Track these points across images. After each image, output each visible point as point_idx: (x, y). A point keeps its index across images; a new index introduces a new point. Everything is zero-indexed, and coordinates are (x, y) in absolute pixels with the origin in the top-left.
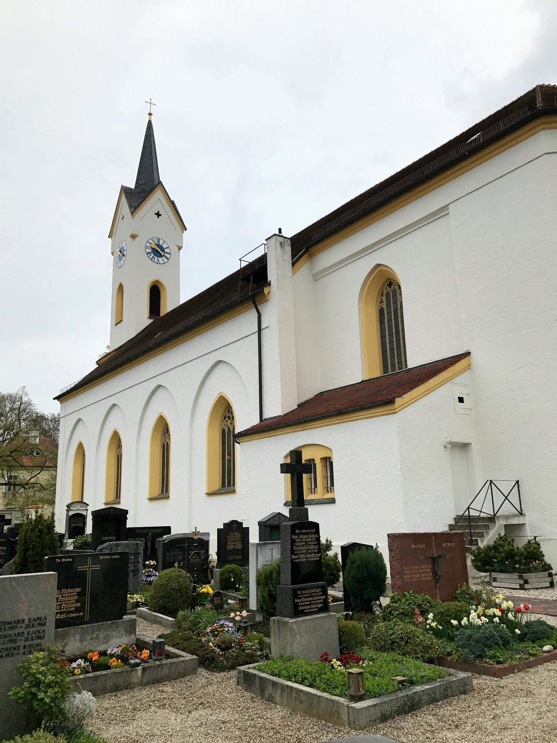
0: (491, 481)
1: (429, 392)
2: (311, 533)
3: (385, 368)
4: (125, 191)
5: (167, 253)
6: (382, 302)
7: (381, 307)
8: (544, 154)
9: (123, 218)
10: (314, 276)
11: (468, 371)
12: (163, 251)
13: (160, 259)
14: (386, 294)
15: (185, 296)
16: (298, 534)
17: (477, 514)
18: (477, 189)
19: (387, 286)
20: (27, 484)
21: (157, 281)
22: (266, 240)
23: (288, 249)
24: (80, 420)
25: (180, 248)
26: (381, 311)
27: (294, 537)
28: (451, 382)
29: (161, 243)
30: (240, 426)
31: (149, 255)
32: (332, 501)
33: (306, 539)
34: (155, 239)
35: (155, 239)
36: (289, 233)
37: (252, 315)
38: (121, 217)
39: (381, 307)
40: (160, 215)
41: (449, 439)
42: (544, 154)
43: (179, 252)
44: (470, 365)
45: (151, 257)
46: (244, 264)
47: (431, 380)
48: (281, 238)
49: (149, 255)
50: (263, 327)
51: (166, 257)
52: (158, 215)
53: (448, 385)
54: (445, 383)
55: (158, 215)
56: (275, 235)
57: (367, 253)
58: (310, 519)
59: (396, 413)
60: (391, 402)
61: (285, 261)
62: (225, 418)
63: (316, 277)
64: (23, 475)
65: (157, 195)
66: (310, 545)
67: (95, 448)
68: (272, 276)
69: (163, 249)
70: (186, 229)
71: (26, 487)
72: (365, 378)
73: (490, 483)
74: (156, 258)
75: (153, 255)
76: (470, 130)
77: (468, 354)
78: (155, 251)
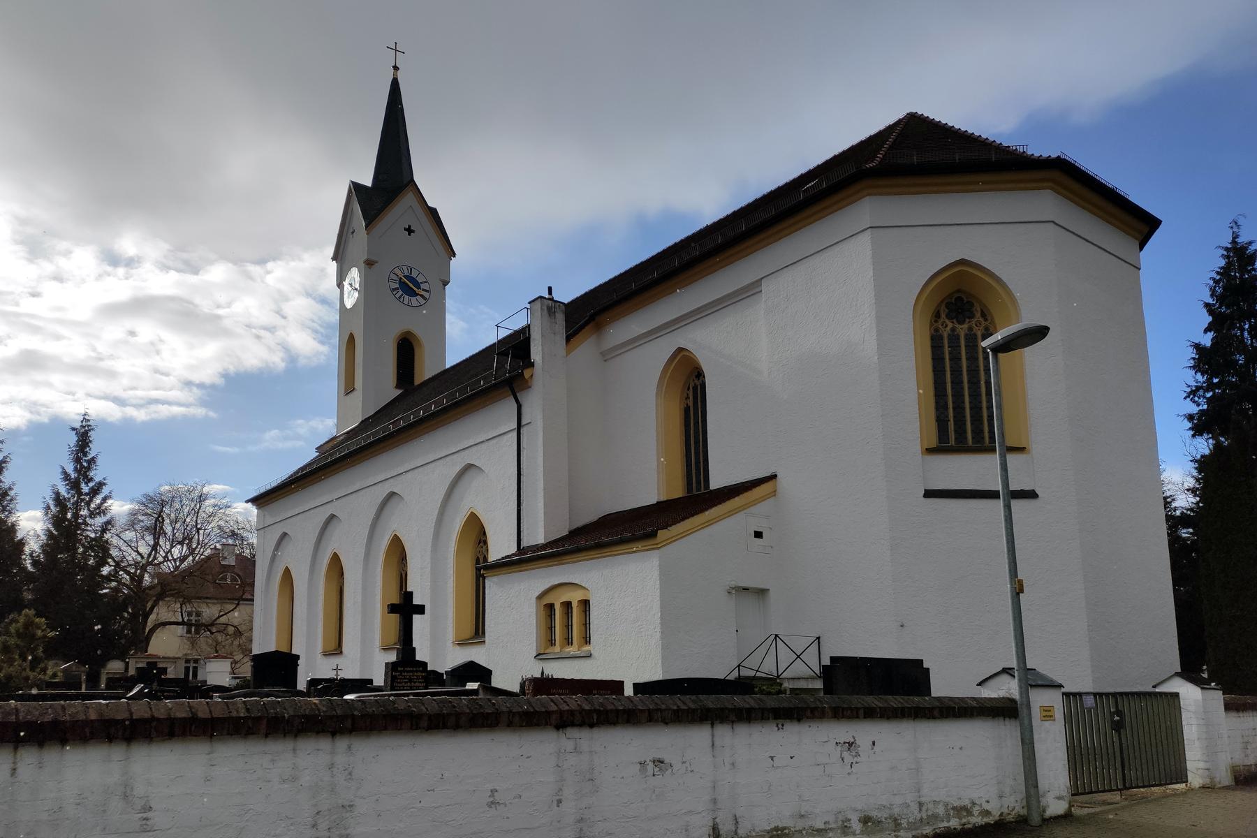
0: (776, 636)
1: (710, 523)
2: (417, 671)
3: (689, 488)
4: (356, 188)
5: (423, 290)
6: (687, 398)
7: (687, 405)
8: (868, 228)
9: (353, 233)
10: (603, 354)
11: (772, 500)
12: (419, 287)
13: (413, 299)
14: (693, 388)
15: (453, 358)
16: (401, 672)
17: (752, 673)
18: (795, 263)
19: (694, 377)
20: (213, 624)
21: (409, 333)
22: (530, 303)
23: (560, 317)
24: (285, 535)
25: (445, 283)
26: (687, 410)
27: (394, 674)
28: (745, 511)
29: (414, 275)
30: (494, 555)
31: (394, 293)
32: (589, 656)
33: (410, 676)
34: (405, 268)
35: (405, 268)
36: (567, 294)
37: (509, 406)
38: (352, 230)
39: (687, 405)
40: (413, 232)
41: (733, 583)
42: (868, 228)
43: (445, 289)
44: (775, 491)
45: (398, 296)
46: (503, 334)
47: (714, 509)
48: (550, 302)
49: (394, 293)
50: (523, 422)
51: (422, 296)
52: (410, 231)
53: (741, 516)
54: (737, 513)
55: (410, 231)
56: (541, 297)
57: (655, 337)
58: (417, 658)
59: (658, 548)
60: (653, 535)
61: (555, 334)
62: (480, 543)
63: (607, 356)
64: (209, 611)
65: (408, 199)
66: (415, 682)
67: (307, 574)
68: (536, 354)
69: (418, 285)
70: (454, 255)
71: (214, 630)
72: (663, 498)
73: (775, 638)
74: (406, 297)
75: (401, 293)
76: (802, 176)
77: (773, 477)
78: (403, 286)
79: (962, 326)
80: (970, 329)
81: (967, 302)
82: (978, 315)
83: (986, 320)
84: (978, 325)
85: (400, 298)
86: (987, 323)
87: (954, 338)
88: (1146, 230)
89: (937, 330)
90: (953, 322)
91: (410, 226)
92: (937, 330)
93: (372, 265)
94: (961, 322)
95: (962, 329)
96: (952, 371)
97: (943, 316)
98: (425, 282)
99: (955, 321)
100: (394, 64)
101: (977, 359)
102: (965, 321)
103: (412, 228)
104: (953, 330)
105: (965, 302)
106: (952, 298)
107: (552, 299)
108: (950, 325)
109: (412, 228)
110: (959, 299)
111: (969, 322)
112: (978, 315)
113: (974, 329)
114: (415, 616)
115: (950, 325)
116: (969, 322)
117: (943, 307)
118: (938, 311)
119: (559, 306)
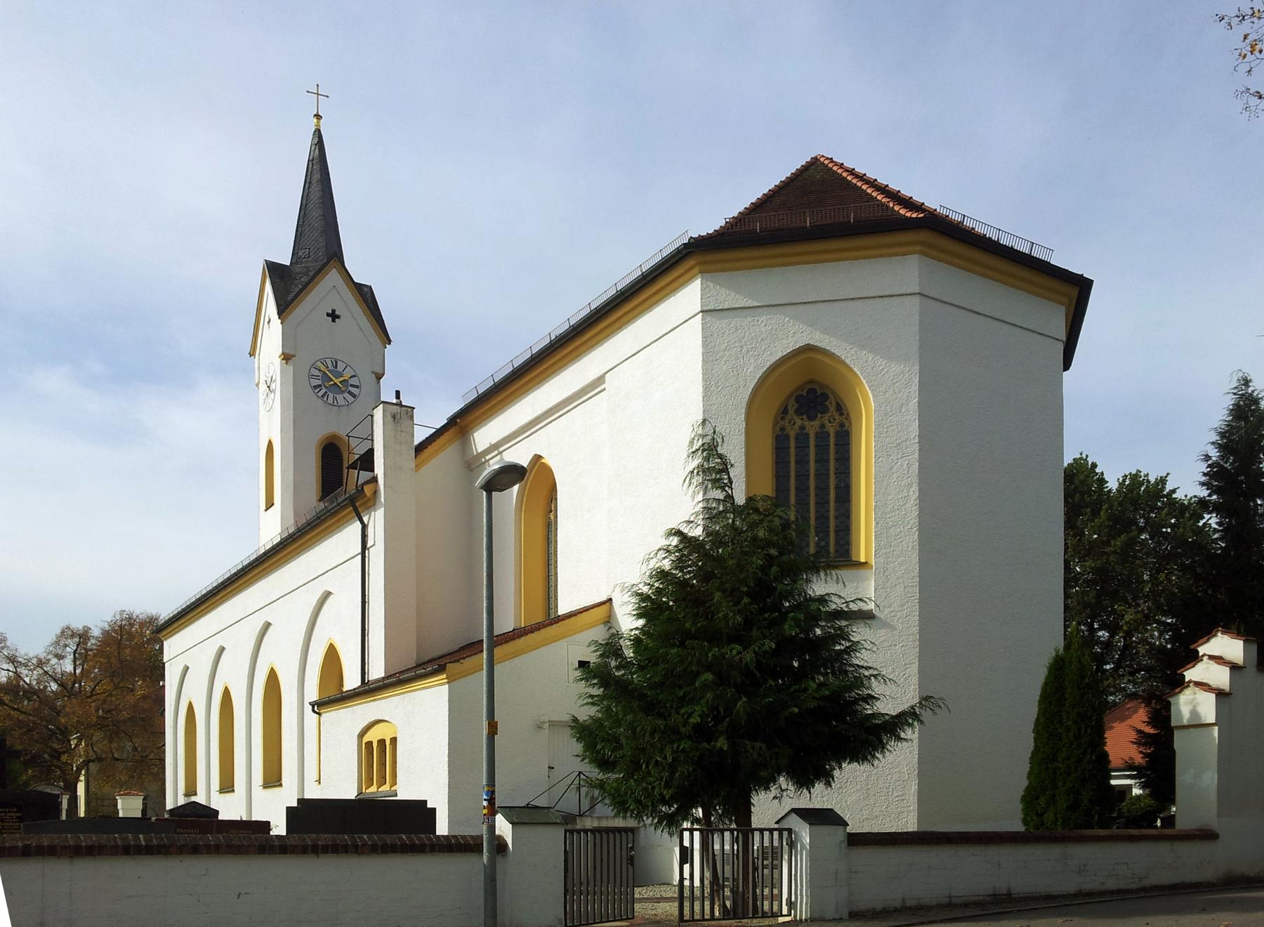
5: (352, 386)
9: (269, 322)
13: (340, 397)
21: (335, 436)
25: (379, 377)
31: (317, 391)
40: (338, 317)
45: (320, 394)
51: (350, 393)
52: (334, 316)
55: (334, 316)
70: (389, 342)
73: (579, 774)
79: (812, 423)
80: (823, 426)
81: (822, 394)
82: (832, 408)
83: (841, 414)
84: (832, 420)
85: (323, 396)
86: (843, 418)
87: (802, 437)
88: (1074, 292)
89: (782, 429)
90: (802, 419)
91: (334, 311)
92: (782, 429)
93: (289, 359)
94: (811, 418)
95: (812, 427)
96: (798, 477)
97: (791, 412)
98: (354, 376)
99: (805, 417)
100: (315, 113)
101: (828, 461)
102: (817, 416)
103: (337, 313)
104: (802, 428)
105: (818, 394)
106: (803, 390)
107: (400, 405)
108: (799, 422)
109: (330, 319)
110: (812, 391)
111: (821, 418)
112: (832, 408)
113: (827, 426)
114: (428, 806)
115: (799, 422)
116: (821, 418)
117: (792, 399)
118: (786, 406)
119: (407, 411)
